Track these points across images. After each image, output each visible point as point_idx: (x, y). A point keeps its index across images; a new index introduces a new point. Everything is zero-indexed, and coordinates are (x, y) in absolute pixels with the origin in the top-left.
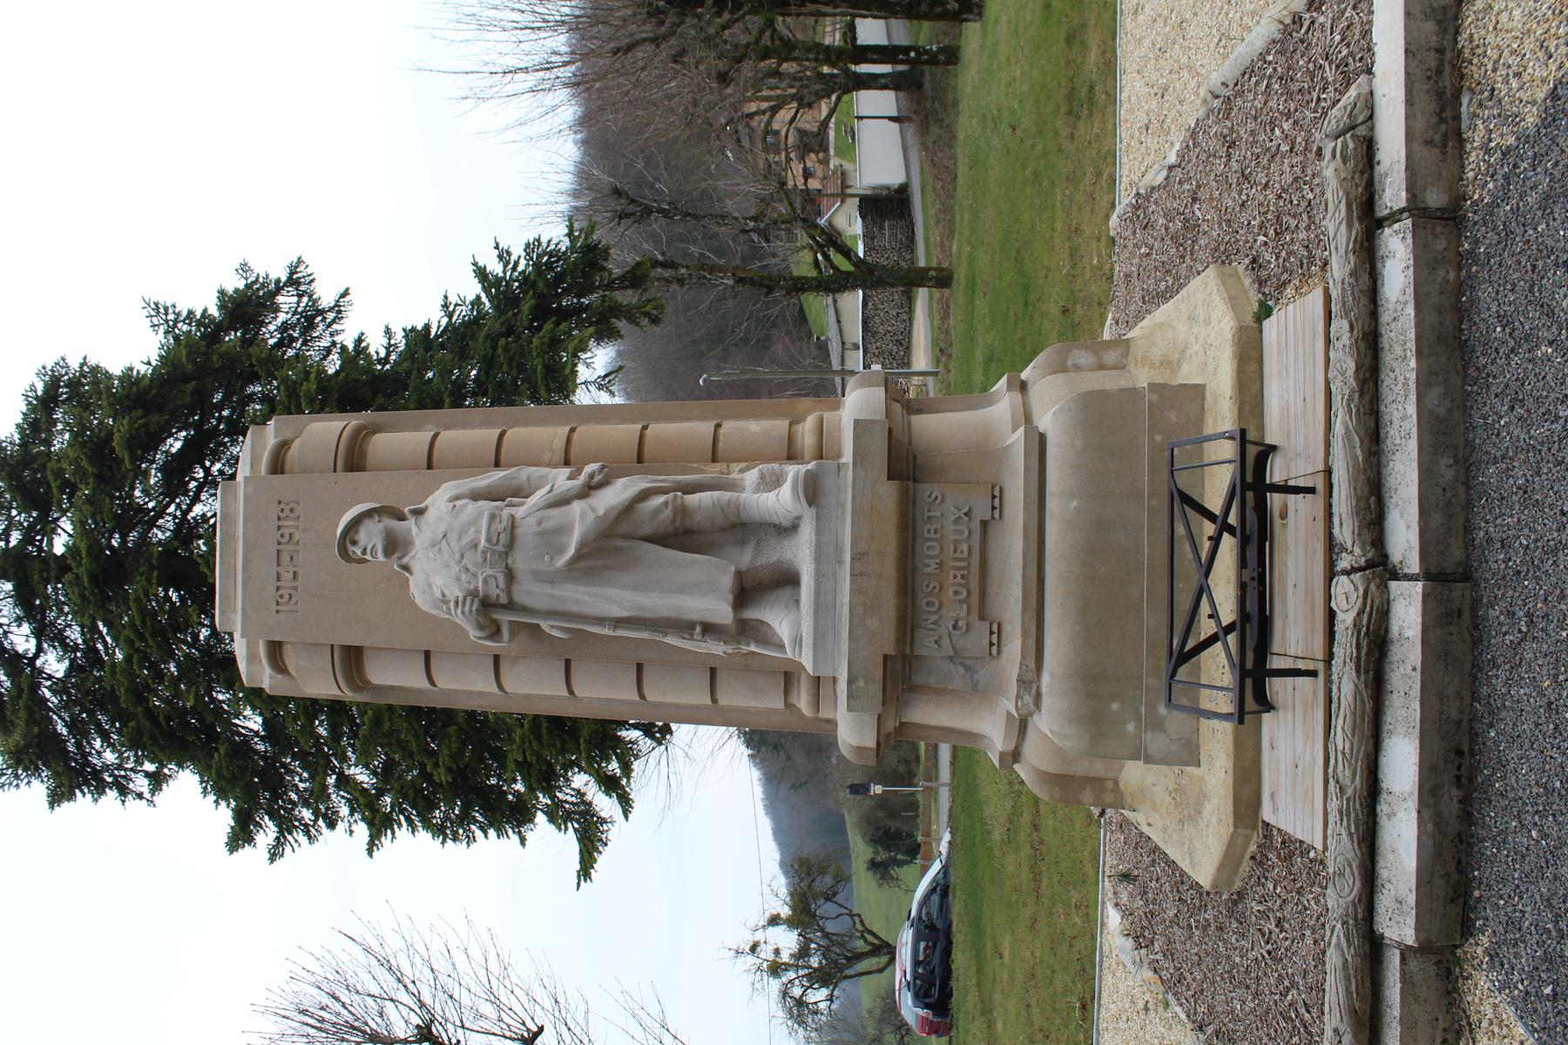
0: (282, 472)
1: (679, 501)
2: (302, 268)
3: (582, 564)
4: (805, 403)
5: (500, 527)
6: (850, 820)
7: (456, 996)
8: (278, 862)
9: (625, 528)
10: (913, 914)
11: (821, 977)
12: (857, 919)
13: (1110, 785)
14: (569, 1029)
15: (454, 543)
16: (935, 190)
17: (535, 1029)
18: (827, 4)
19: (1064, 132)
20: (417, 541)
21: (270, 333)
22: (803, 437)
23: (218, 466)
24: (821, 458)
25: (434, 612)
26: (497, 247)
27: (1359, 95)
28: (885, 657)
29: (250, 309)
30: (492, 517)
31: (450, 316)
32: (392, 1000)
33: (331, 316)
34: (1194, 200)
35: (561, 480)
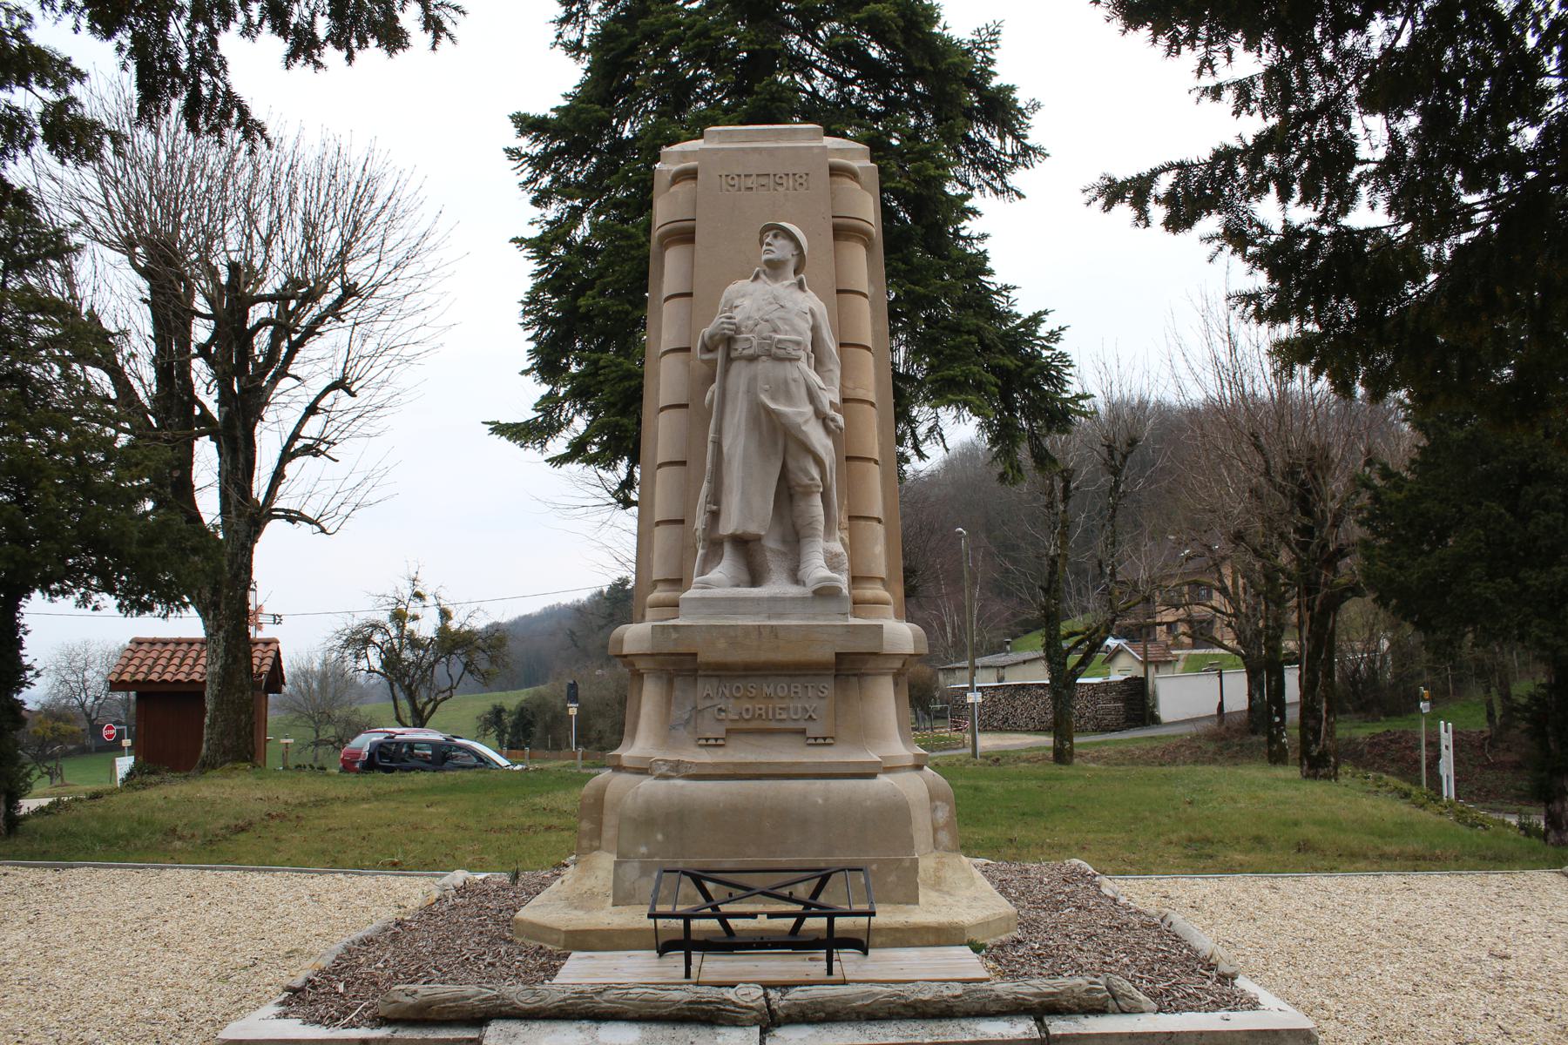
0: (831, 175)
2: (1039, 158)
5: (790, 350)
7: (382, 317)
8: (505, 155)
9: (792, 447)
10: (458, 741)
11: (391, 661)
12: (447, 694)
13: (596, 843)
14: (354, 420)
15: (777, 314)
16: (1153, 749)
17: (353, 389)
18: (1310, 631)
19: (1174, 837)
20: (777, 286)
21: (978, 131)
23: (857, 90)
25: (723, 300)
26: (1061, 329)
27: (1140, 1001)
29: (1000, 115)
30: (798, 343)
31: (998, 293)
32: (379, 261)
33: (998, 184)
34: (1079, 908)
35: (830, 395)
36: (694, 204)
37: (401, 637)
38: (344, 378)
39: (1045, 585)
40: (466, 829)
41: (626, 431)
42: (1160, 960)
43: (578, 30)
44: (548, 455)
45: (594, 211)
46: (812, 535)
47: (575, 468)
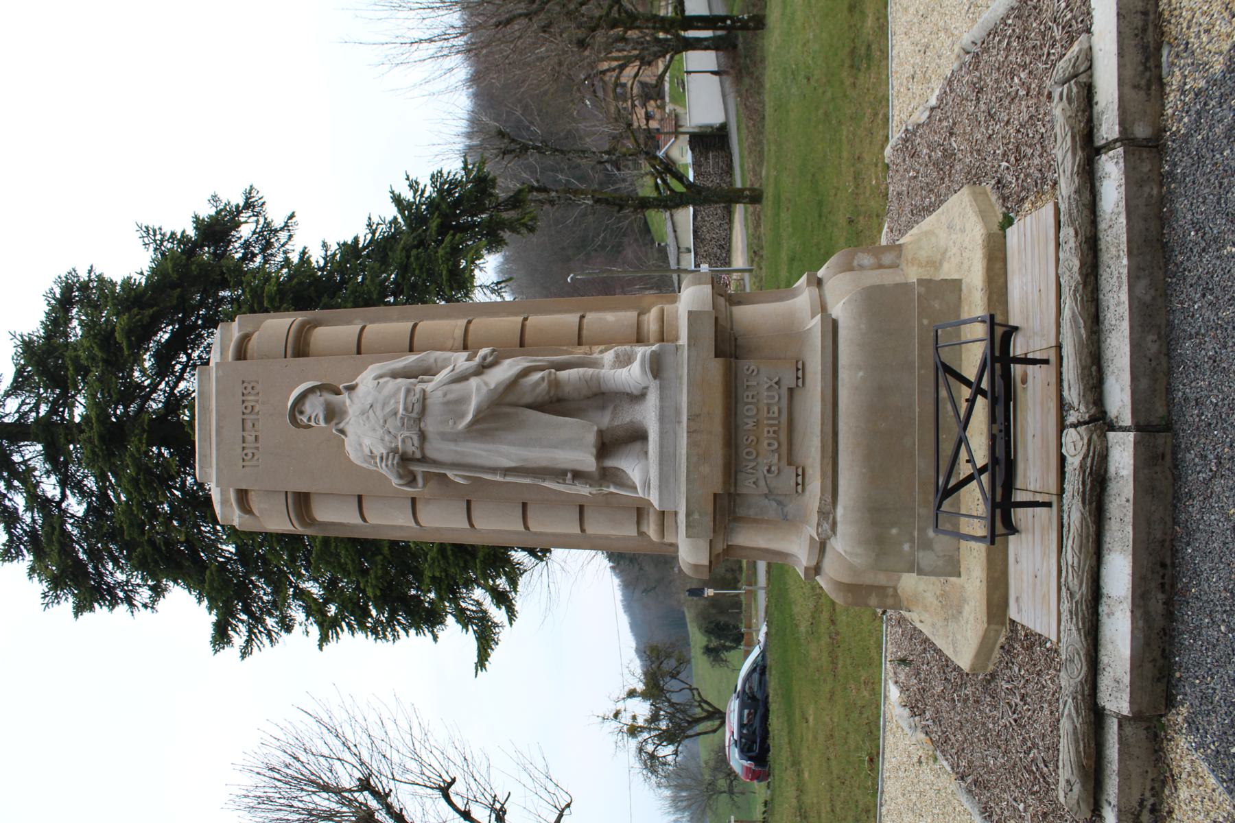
1: (553, 376)
3: (478, 427)
4: (649, 296)
5: (414, 399)
6: (689, 616)
7: (388, 755)
9: (511, 398)
10: (739, 688)
11: (669, 737)
12: (695, 692)
13: (890, 591)
15: (379, 412)
16: (748, 128)
17: (449, 780)
19: (848, 82)
20: (350, 411)
22: (649, 325)
24: (663, 340)
25: (365, 465)
26: (408, 179)
27: (1080, 51)
28: (715, 495)
30: (408, 391)
31: (374, 233)
32: (339, 759)
34: (951, 134)
35: (461, 361)
36: (270, 493)
37: (650, 729)
38: (440, 789)
39: (617, 208)
40: (832, 693)
41: (489, 554)
42: (1022, 44)
43: (140, 590)
44: (506, 622)
45: (298, 579)
46: (598, 380)
47: (519, 604)
